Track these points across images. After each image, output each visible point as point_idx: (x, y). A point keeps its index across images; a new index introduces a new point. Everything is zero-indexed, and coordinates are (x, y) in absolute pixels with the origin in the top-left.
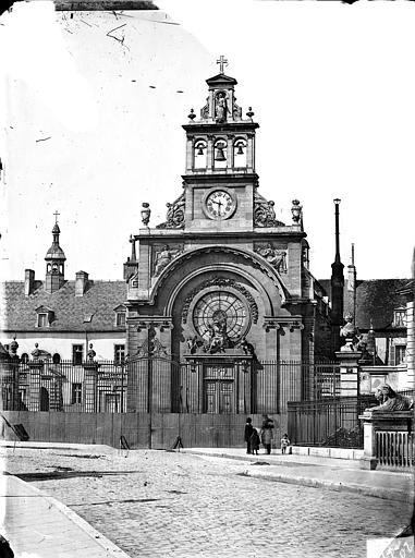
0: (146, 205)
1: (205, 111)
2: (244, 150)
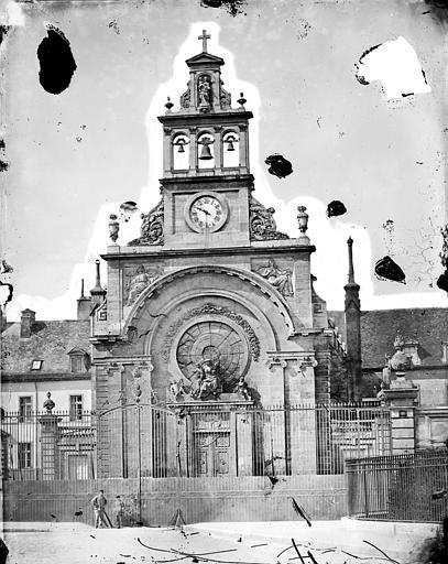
0: (303, 209)
1: (185, 98)
2: (236, 145)
